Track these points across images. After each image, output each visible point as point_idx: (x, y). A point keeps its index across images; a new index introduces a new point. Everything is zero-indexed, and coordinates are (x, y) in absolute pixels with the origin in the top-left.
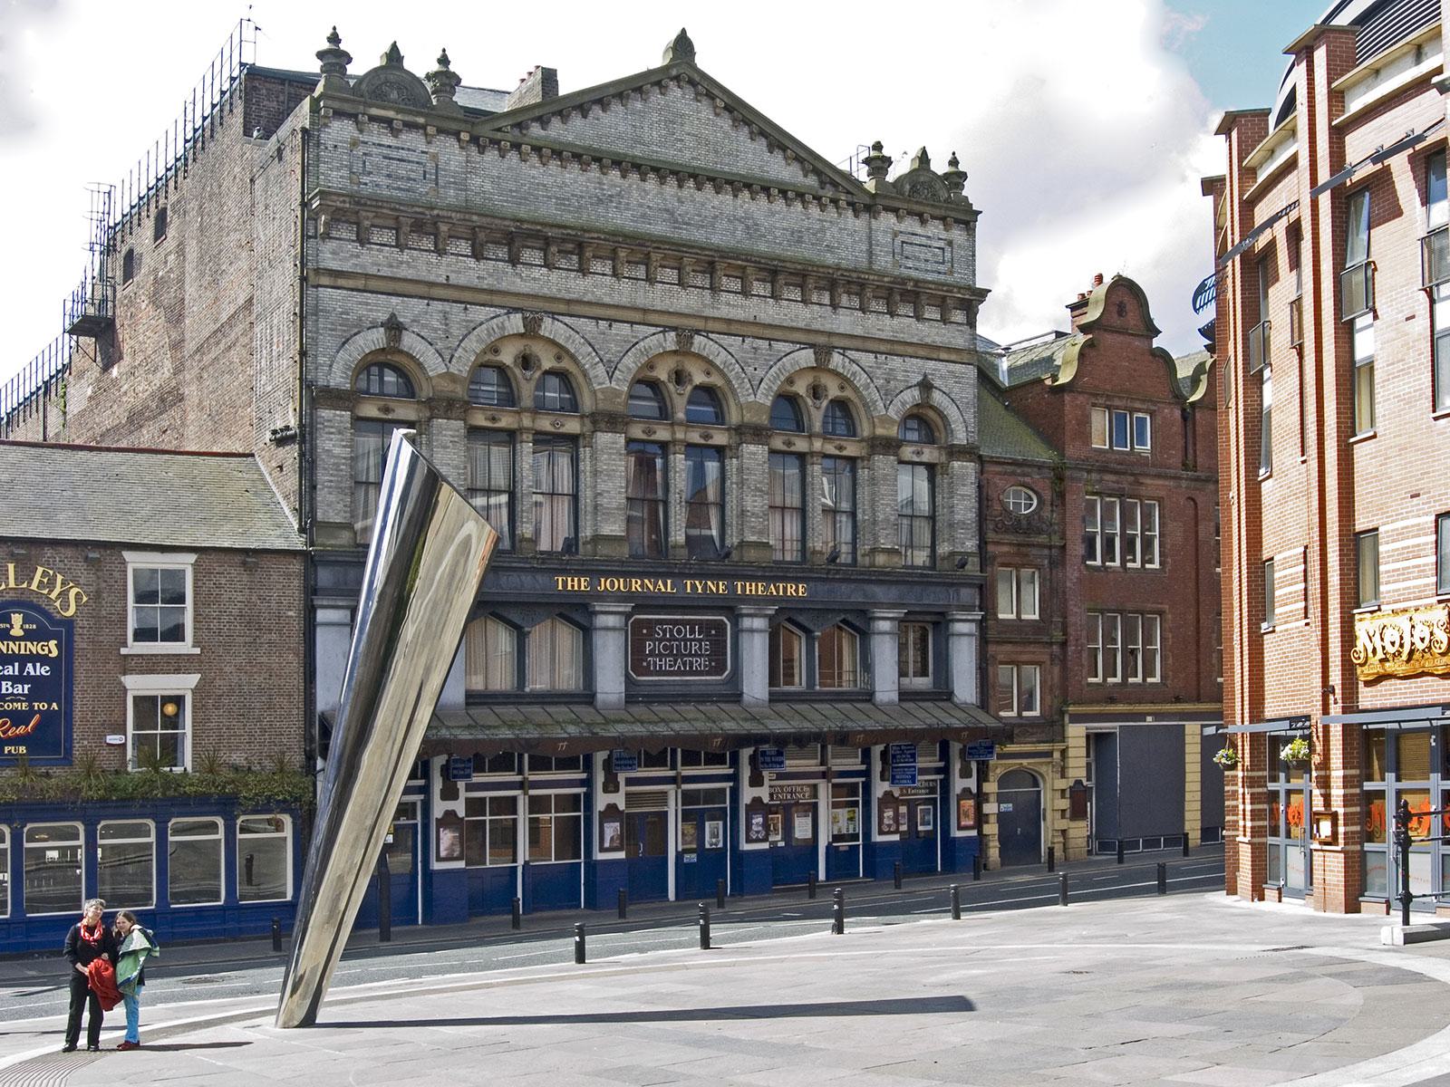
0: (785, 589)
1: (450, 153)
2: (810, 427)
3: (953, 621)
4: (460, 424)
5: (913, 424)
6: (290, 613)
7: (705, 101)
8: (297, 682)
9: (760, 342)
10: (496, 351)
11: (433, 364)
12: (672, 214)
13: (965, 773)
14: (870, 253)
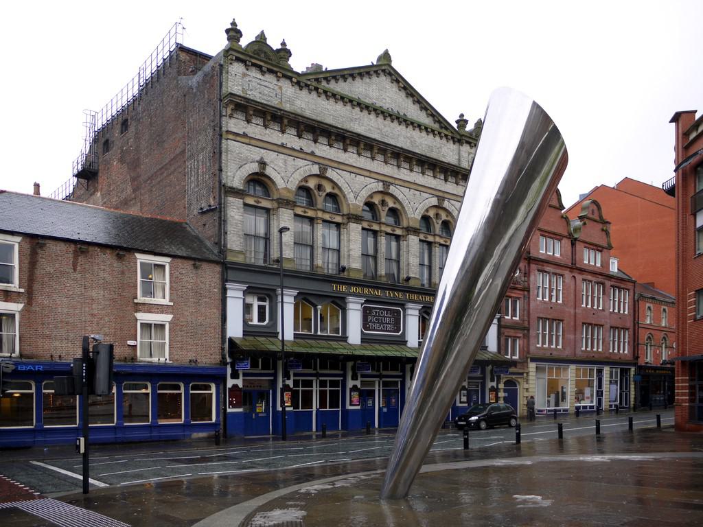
0: (425, 298)
1: (288, 89)
2: (434, 231)
3: (409, 308)
4: (292, 211)
5: (301, 192)
6: (215, 290)
7: (395, 84)
8: (219, 322)
9: (416, 192)
10: (307, 181)
11: (280, 184)
12: (381, 131)
13: (492, 380)
14: (459, 160)
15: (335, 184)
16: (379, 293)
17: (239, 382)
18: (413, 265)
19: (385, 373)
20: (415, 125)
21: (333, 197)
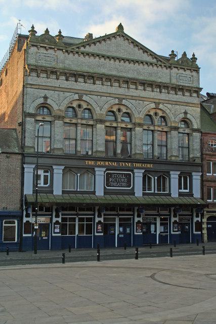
7: (126, 41)
8: (19, 186)
11: (55, 107)
13: (197, 216)
15: (164, 112)
16: (115, 164)
17: (141, 219)
18: (139, 146)
19: (121, 213)
20: (85, 54)
21: (128, 115)
